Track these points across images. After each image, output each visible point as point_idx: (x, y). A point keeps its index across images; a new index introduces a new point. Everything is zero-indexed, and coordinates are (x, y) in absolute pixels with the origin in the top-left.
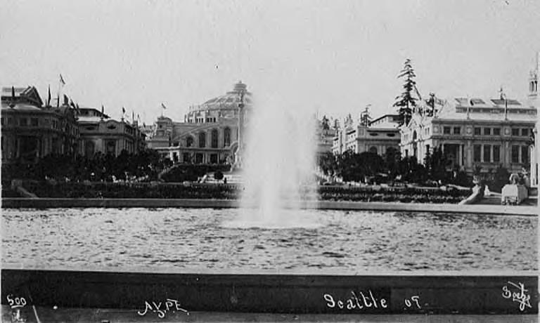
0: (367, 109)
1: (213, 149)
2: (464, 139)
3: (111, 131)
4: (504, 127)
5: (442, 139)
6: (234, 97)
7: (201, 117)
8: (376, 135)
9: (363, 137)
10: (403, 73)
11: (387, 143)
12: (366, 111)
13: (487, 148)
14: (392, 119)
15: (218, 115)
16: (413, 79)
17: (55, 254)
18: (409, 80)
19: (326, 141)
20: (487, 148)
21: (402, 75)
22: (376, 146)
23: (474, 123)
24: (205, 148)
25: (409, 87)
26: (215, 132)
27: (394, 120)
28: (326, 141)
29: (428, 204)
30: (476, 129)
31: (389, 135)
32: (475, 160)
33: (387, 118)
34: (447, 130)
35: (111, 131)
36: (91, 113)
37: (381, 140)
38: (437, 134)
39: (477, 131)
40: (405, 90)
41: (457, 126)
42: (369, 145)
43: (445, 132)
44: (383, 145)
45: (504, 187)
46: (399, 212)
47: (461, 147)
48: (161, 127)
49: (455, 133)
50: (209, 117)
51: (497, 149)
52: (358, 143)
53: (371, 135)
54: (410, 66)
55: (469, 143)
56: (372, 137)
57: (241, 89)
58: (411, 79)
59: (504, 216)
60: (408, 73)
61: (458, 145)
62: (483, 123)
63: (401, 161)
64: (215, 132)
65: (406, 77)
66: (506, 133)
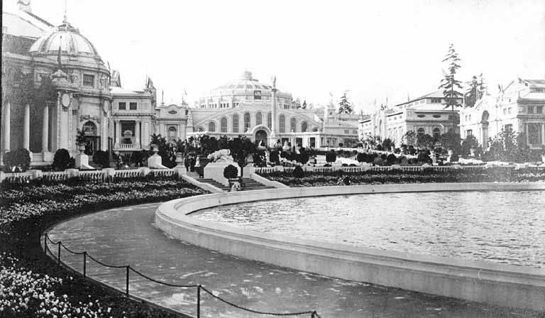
0: (345, 94)
1: (287, 137)
3: (171, 116)
7: (214, 103)
8: (423, 116)
9: (412, 119)
10: (449, 56)
11: (433, 124)
12: (345, 97)
14: (430, 100)
15: (231, 100)
16: (457, 63)
17: (263, 207)
22: (175, 126)
24: (215, 132)
26: (236, 118)
27: (432, 102)
31: (435, 116)
35: (171, 116)
37: (428, 121)
43: (120, 109)
44: (429, 126)
45: (207, 166)
48: (331, 114)
49: (131, 109)
50: (222, 103)
54: (453, 50)
56: (419, 119)
57: (150, 82)
58: (455, 62)
59: (272, 202)
64: (236, 118)
65: (451, 60)
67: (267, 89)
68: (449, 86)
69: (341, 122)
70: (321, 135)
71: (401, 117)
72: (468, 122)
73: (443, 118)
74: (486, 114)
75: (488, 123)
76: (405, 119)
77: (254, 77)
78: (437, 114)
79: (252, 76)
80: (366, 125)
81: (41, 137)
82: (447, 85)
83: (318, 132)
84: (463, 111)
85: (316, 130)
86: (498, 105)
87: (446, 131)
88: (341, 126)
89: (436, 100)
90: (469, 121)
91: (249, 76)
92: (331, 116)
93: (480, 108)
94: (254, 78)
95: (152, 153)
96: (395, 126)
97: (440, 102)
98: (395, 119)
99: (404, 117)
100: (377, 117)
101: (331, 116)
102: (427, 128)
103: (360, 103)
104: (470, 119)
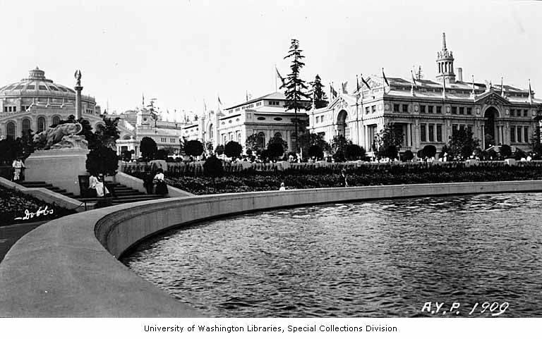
2: (413, 118)
4: (446, 105)
5: (393, 117)
6: (34, 83)
8: (264, 119)
10: (292, 53)
13: (431, 127)
14: (267, 102)
18: (296, 61)
19: (156, 132)
20: (431, 127)
21: (289, 56)
23: (420, 100)
25: (295, 68)
27: (270, 103)
28: (156, 132)
29: (243, 220)
30: (421, 106)
32: (422, 140)
33: (262, 102)
34: (396, 108)
36: (404, 89)
38: (388, 112)
39: (422, 109)
40: (291, 71)
41: (405, 103)
42: (291, 131)
46: (398, 201)
47: (409, 126)
51: (439, 127)
52: (246, 128)
53: (259, 119)
55: (417, 121)
58: (299, 60)
60: (297, 53)
61: (406, 124)
62: (427, 101)
63: (233, 157)
65: (293, 58)
66: (414, 110)
67: (57, 90)
68: (293, 86)
69: (157, 129)
70: (134, 142)
71: (238, 120)
72: (320, 124)
73: (286, 121)
74: (343, 114)
75: (345, 125)
76: (244, 121)
77: (47, 76)
78: (278, 117)
79: (45, 75)
80: (192, 130)
81: (430, 130)
82: (290, 84)
83: (132, 140)
84: (313, 113)
85: (128, 138)
86: (359, 102)
87: (272, 136)
88: (157, 134)
89: (273, 102)
90: (322, 124)
91: (39, 75)
92: (145, 122)
93: (336, 107)
94: (47, 78)
95: (304, 132)
96: (230, 130)
97: (278, 104)
98: (230, 122)
99: (243, 119)
100: (206, 121)
101: (145, 122)
102: (285, 132)
103: (196, 118)
104: (322, 121)
